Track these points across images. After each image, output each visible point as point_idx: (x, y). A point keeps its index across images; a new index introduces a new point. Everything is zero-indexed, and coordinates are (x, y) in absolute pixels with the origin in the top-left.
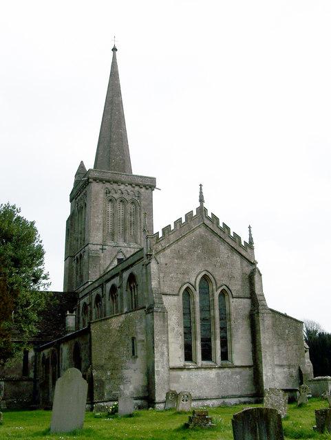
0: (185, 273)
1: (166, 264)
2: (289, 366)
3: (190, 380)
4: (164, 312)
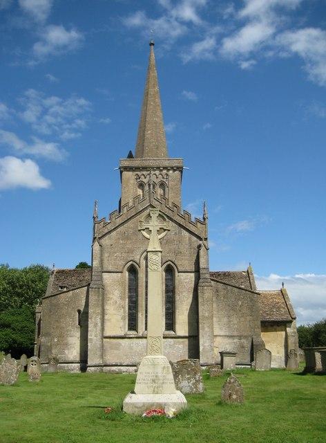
0: (131, 251)
1: (111, 245)
2: (240, 337)
3: (131, 348)
4: (102, 289)
